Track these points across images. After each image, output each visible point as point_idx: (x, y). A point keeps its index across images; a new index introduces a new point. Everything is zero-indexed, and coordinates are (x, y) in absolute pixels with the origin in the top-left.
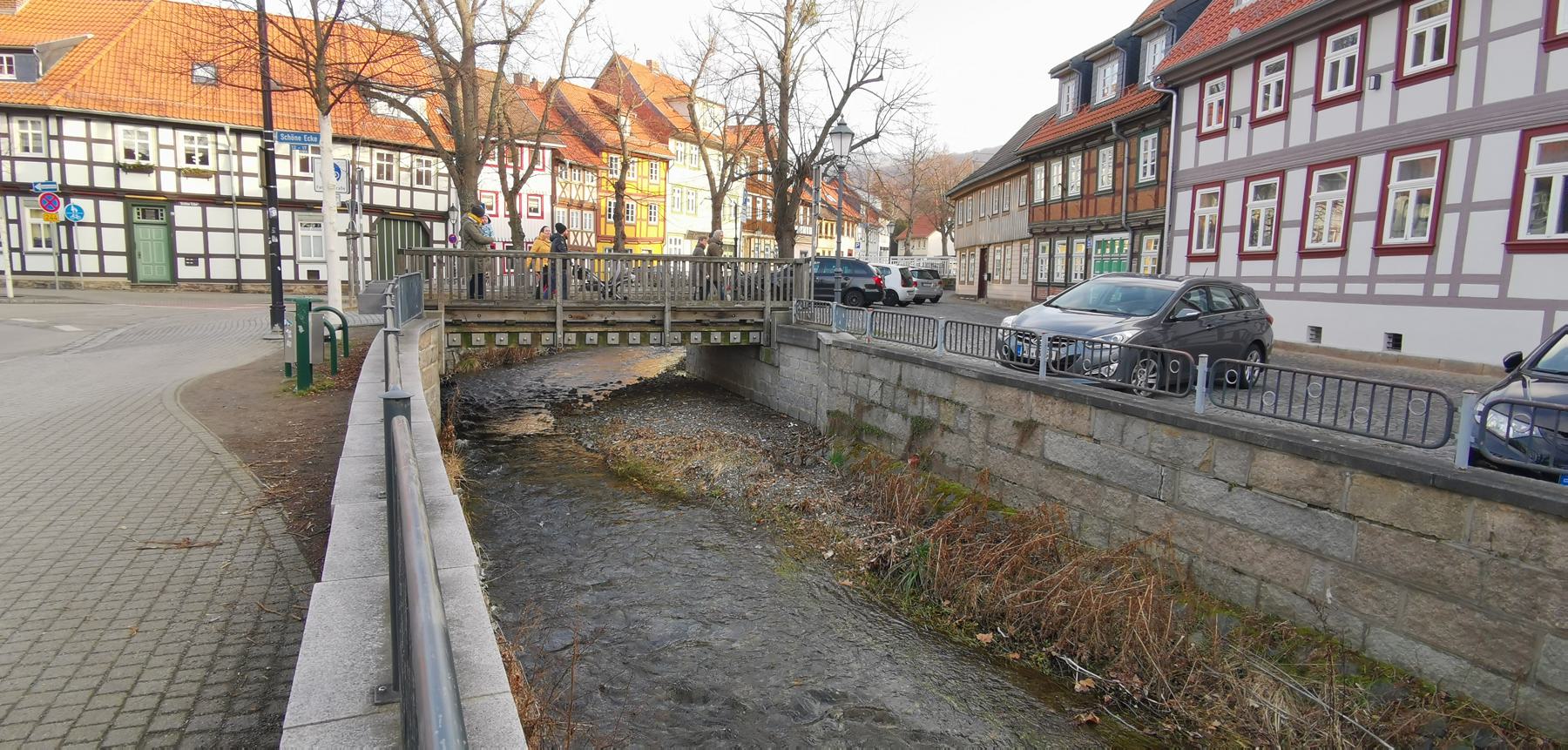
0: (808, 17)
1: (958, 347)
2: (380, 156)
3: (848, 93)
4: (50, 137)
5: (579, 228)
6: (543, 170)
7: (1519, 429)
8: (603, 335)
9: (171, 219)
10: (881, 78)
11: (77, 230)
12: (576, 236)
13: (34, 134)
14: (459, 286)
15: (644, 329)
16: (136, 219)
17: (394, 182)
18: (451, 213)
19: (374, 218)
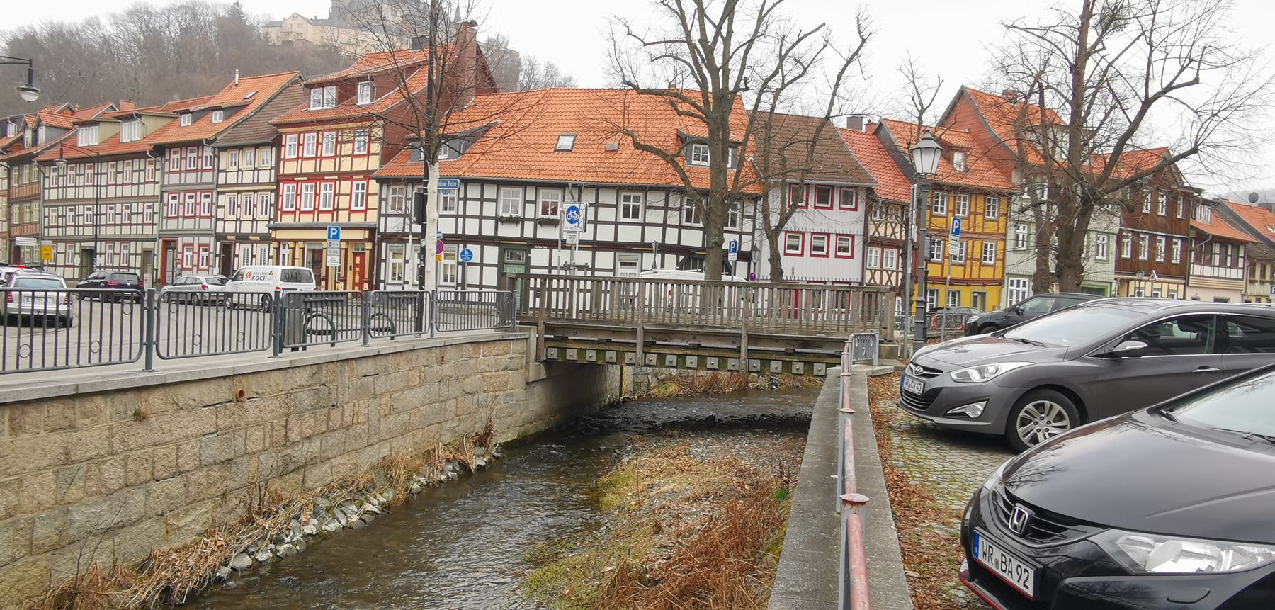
0: (1112, 21)
1: (240, 344)
2: (627, 198)
3: (1147, 103)
4: (460, 199)
5: (878, 267)
6: (806, 207)
7: (456, 502)
8: (682, 357)
9: (528, 259)
10: (1196, 81)
11: (469, 268)
12: (890, 276)
13: (633, 206)
14: (715, 317)
15: (722, 354)
16: (506, 260)
17: (737, 229)
18: (753, 253)
19: (681, 258)
